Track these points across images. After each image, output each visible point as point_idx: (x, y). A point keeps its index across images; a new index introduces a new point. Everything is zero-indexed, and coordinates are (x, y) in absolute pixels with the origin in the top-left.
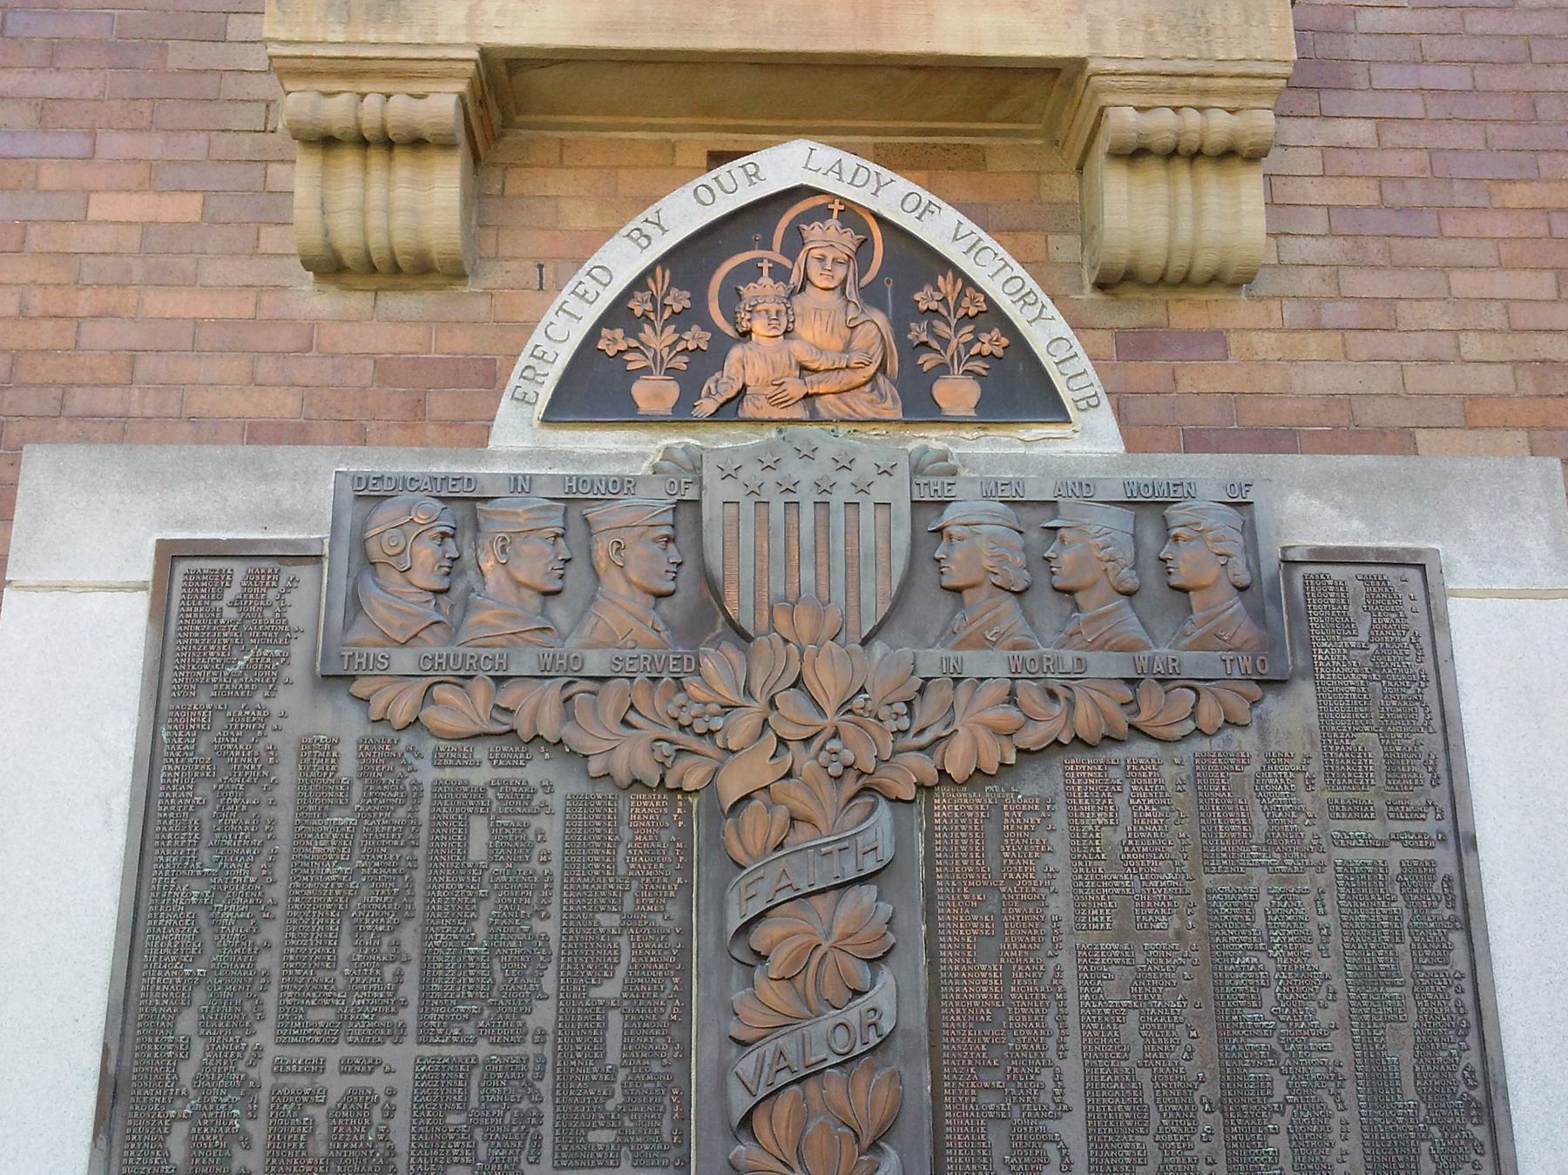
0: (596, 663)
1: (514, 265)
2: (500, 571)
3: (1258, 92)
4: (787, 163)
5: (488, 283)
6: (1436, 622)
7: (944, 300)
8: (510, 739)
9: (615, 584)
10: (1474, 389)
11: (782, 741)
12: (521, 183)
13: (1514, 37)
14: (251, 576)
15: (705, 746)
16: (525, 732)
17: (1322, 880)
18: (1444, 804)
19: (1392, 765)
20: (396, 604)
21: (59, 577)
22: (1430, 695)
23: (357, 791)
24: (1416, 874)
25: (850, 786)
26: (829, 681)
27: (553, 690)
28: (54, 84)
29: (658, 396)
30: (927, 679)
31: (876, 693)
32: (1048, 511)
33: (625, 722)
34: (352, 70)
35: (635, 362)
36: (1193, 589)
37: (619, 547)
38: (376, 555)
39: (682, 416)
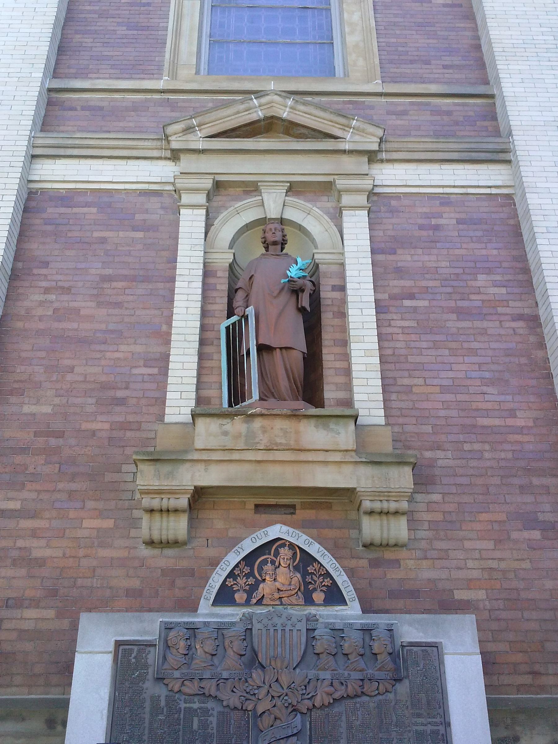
0: (225, 675)
1: (200, 539)
2: (201, 649)
3: (403, 496)
4: (276, 531)
5: (193, 545)
6: (441, 662)
7: (315, 570)
8: (204, 696)
9: (230, 652)
10: (470, 577)
11: (273, 697)
12: (203, 514)
13: (482, 468)
14: (139, 651)
15: (253, 698)
16: (207, 694)
17: (410, 735)
18: (442, 714)
19: (428, 703)
20: (174, 658)
21: (90, 649)
22: (439, 683)
23: (165, 709)
24: (435, 733)
25: (290, 709)
26: (285, 680)
27: (214, 682)
28: (74, 486)
29: (241, 598)
30: (310, 679)
31: (297, 682)
32: (341, 632)
33: (232, 691)
34: (159, 492)
35: (236, 588)
36: (378, 654)
37: (231, 642)
38: (170, 645)
39: (247, 603)
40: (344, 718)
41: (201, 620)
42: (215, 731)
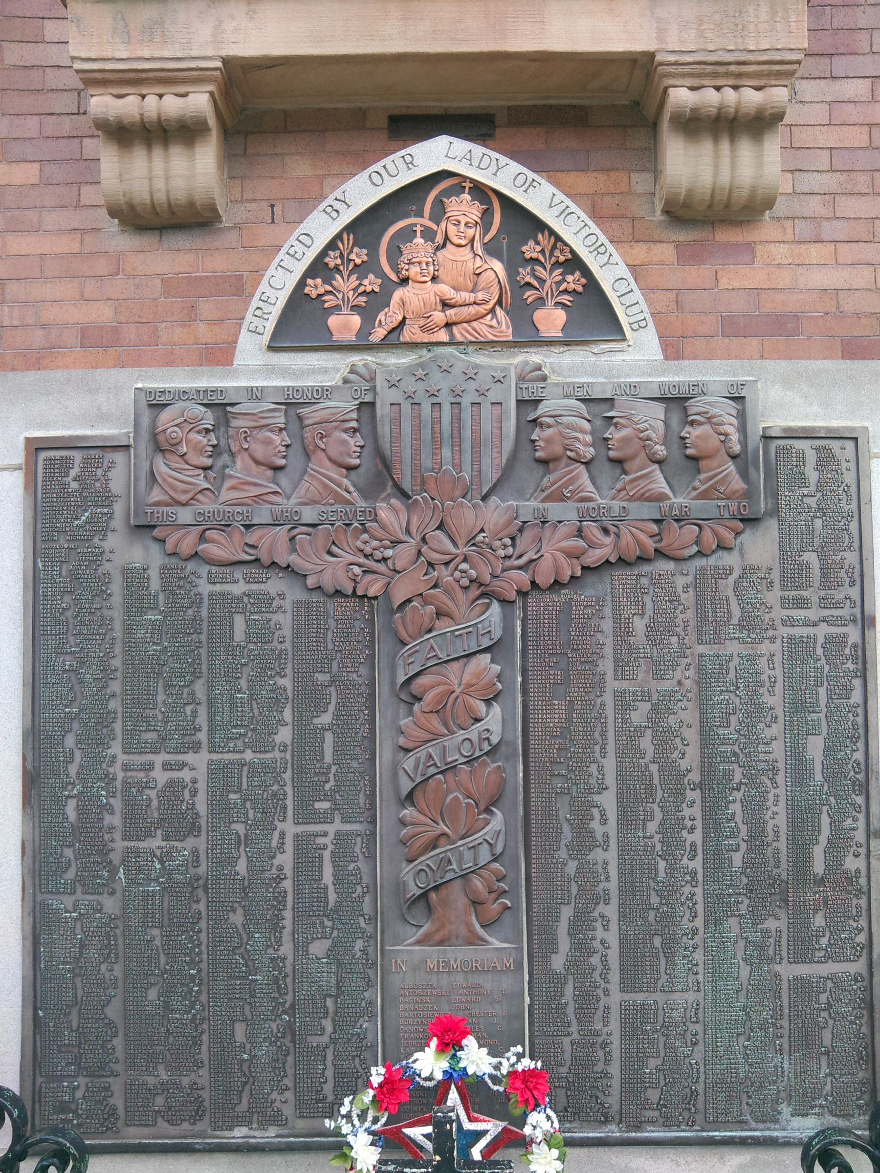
0: (309, 515)
11: (431, 565)
14: (85, 460)
15: (381, 567)
22: (853, 526)
23: (161, 598)
25: (475, 592)
27: (282, 532)
32: (607, 406)
40: (608, 611)
41: (242, 385)
42: (288, 645)
